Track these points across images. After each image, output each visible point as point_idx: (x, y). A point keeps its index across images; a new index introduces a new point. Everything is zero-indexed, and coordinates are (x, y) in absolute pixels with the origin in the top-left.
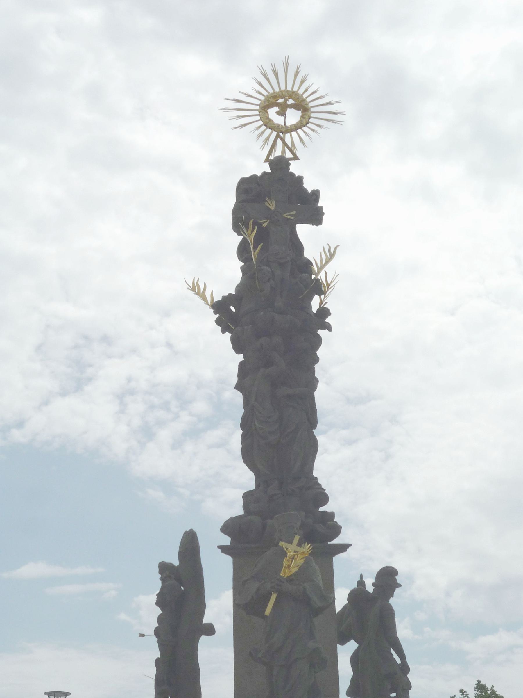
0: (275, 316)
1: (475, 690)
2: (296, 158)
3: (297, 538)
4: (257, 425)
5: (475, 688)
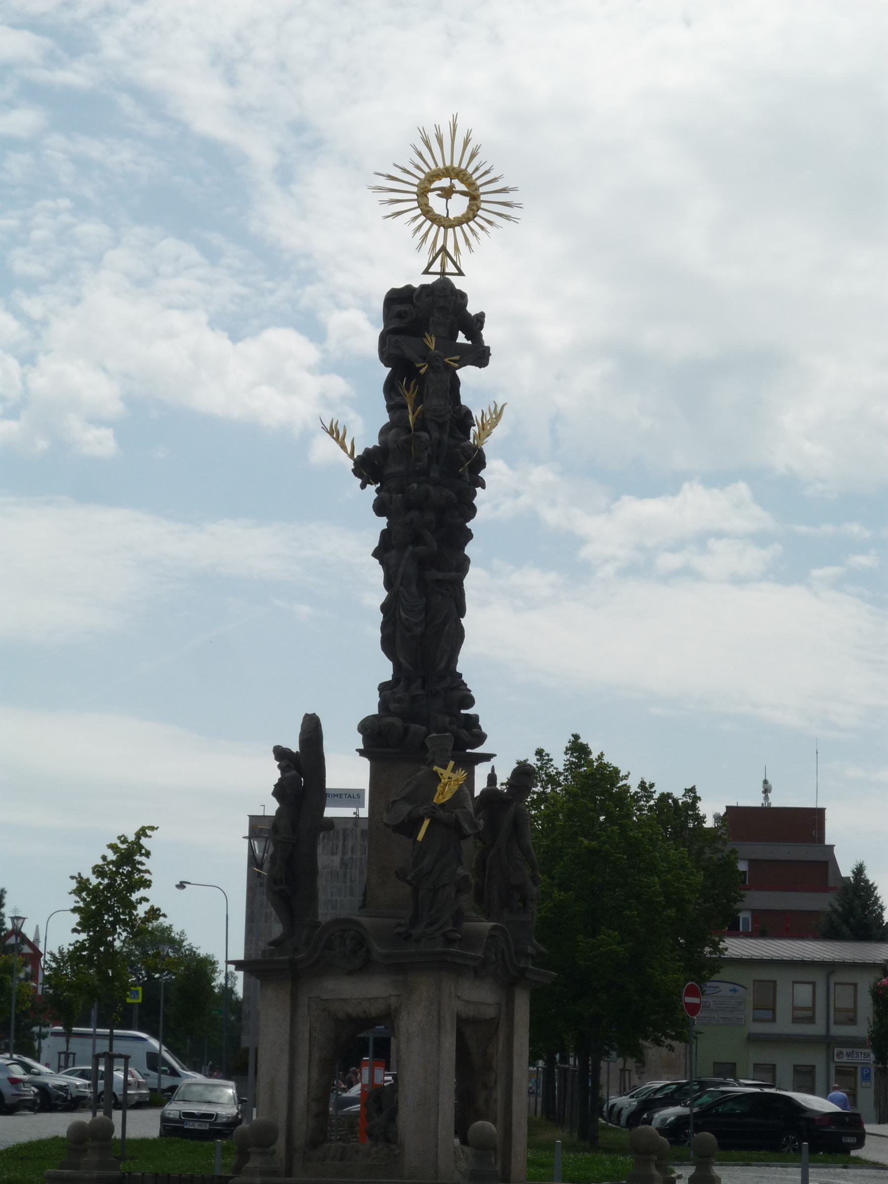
0: (425, 476)
1: (566, 754)
2: (461, 273)
3: (452, 763)
4: (403, 615)
5: (567, 749)
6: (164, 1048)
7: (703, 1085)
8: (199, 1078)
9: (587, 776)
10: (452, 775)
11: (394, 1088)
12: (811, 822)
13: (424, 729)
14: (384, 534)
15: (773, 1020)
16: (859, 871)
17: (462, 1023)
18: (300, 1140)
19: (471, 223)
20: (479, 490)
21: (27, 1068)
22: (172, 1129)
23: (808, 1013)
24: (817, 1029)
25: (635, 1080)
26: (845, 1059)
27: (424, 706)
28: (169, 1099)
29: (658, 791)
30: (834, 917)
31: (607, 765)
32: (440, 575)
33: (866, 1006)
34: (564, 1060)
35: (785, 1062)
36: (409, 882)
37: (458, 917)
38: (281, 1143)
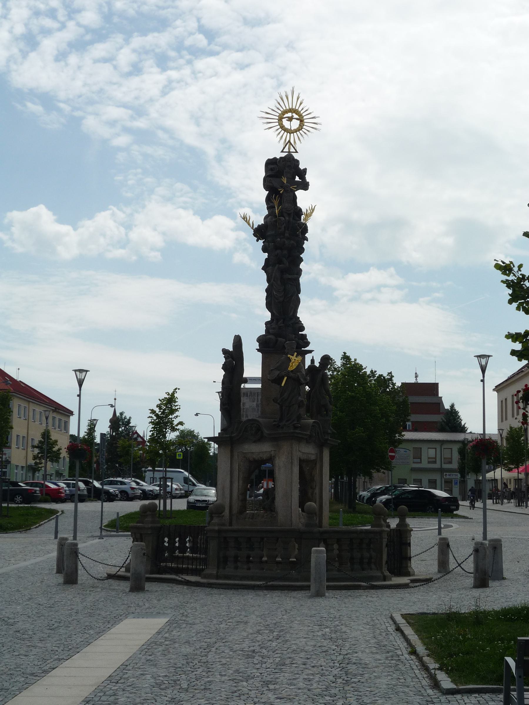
0: (283, 236)
2: (296, 152)
3: (296, 354)
6: (190, 475)
7: (396, 487)
8: (203, 486)
9: (349, 368)
10: (296, 358)
11: (274, 489)
12: (433, 388)
13: (284, 340)
14: (266, 260)
15: (421, 462)
16: (452, 406)
17: (301, 461)
18: (235, 510)
19: (301, 131)
20: (305, 241)
21: (138, 484)
22: (191, 506)
23: (434, 460)
24: (437, 466)
25: (369, 486)
26: (448, 477)
27: (284, 333)
28: (190, 495)
29: (378, 373)
30: (443, 423)
31: (358, 364)
32: (290, 277)
33: (456, 456)
34: (342, 478)
35: (425, 478)
36: (279, 404)
37: (299, 418)
38: (227, 512)
